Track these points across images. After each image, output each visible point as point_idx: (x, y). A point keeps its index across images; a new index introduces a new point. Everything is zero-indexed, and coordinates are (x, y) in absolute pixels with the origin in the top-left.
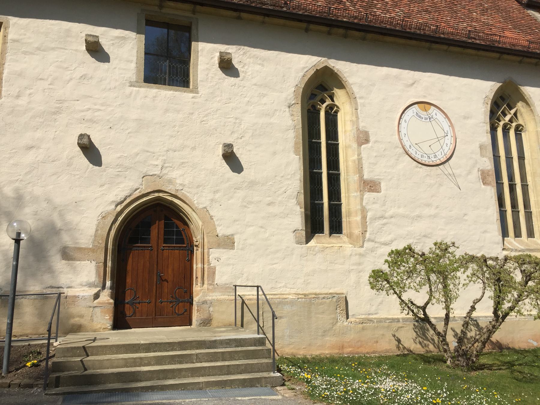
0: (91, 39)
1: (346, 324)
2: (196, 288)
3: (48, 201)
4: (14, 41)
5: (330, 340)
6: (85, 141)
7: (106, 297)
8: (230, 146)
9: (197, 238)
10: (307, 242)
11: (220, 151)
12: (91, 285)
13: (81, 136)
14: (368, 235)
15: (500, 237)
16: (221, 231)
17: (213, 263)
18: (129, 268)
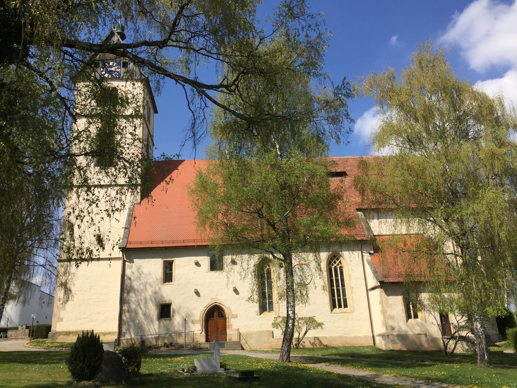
0: (196, 262)
1: (272, 340)
2: (228, 330)
3: (188, 308)
4: (177, 265)
5: (267, 345)
6: (196, 291)
7: (203, 333)
8: (234, 288)
9: (227, 316)
10: (260, 315)
11: (232, 289)
12: (200, 330)
13: (195, 290)
14: (280, 311)
15: (330, 309)
16: (234, 313)
17: (232, 323)
18: (209, 325)
